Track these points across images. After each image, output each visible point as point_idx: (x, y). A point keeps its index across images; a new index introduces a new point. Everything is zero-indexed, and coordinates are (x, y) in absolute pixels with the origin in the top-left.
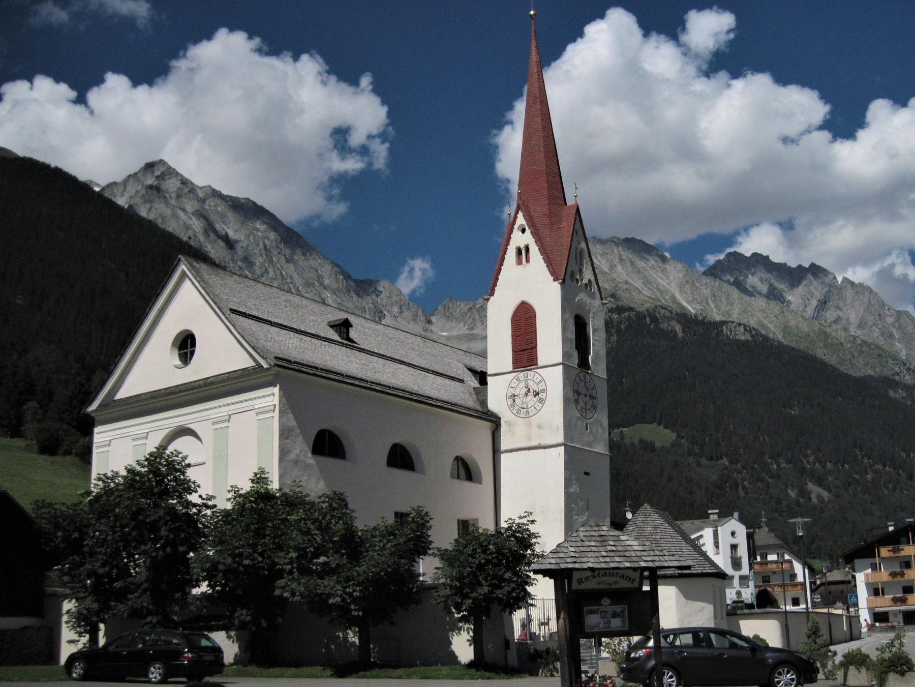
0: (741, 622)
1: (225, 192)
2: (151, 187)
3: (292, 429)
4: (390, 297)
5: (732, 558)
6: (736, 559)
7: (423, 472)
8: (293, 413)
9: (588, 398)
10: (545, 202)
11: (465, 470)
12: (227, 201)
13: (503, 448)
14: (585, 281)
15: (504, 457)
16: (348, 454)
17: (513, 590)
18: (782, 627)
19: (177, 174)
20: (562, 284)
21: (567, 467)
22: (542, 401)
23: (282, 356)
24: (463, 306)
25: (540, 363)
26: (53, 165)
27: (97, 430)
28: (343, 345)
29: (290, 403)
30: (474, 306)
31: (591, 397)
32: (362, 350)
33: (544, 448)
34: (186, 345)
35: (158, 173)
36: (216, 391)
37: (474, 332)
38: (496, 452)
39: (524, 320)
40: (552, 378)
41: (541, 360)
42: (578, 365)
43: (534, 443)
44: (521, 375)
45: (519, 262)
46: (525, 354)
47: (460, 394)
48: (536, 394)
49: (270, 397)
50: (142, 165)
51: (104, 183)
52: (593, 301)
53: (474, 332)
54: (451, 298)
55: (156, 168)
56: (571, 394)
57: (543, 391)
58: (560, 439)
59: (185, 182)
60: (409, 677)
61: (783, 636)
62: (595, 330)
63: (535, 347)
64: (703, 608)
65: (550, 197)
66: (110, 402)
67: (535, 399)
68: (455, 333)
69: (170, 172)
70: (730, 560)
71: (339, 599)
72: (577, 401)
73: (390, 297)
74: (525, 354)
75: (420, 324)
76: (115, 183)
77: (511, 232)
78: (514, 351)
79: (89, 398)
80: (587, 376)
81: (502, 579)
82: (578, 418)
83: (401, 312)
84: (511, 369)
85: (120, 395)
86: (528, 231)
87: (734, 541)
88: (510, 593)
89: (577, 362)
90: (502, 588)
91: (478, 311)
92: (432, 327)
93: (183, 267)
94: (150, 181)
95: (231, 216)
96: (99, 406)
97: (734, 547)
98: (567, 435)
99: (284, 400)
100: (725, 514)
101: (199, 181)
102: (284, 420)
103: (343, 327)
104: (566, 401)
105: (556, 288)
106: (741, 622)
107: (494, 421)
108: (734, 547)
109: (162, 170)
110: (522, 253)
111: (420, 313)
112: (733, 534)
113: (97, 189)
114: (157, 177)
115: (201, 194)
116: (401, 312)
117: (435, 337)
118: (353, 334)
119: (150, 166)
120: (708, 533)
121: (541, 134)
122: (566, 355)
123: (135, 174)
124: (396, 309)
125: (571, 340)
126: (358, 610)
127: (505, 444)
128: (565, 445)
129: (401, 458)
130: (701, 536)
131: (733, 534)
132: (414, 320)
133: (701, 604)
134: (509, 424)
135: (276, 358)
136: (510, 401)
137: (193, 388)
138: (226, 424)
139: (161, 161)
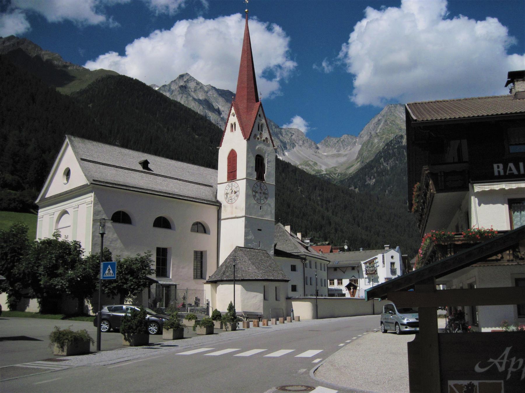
0: (293, 302)
1: (217, 88)
2: (182, 86)
3: (100, 212)
4: (298, 136)
5: (391, 269)
6: (394, 269)
7: (175, 230)
8: (101, 204)
9: (262, 194)
10: (245, 101)
11: (201, 228)
12: (218, 92)
13: (222, 218)
14: (264, 138)
15: (222, 222)
16: (133, 221)
17: (132, 285)
18: (313, 306)
19: (194, 80)
20: (247, 141)
21: (246, 227)
22: (237, 196)
23: (97, 179)
24: (334, 140)
25: (238, 178)
26: (134, 79)
27: (39, 211)
28: (144, 172)
29: (99, 200)
30: (340, 140)
31: (264, 193)
32: (156, 175)
33: (237, 218)
34: (68, 173)
35: (185, 80)
36: (74, 195)
37: (340, 152)
38: (219, 219)
39: (232, 157)
40: (241, 185)
41: (238, 177)
42: (256, 179)
43: (234, 216)
44: (230, 184)
45: (232, 131)
46: (232, 175)
47: (204, 193)
48: (235, 193)
49: (90, 197)
50: (178, 76)
51: (161, 85)
52: (268, 148)
53: (340, 152)
54: (328, 136)
55: (184, 77)
56: (250, 192)
57: (238, 191)
58: (243, 214)
59: (198, 83)
60: (76, 320)
61: (313, 310)
62: (268, 162)
63: (236, 171)
64: (257, 296)
65: (248, 99)
66: (43, 199)
67: (235, 195)
68: (330, 153)
69: (191, 79)
70: (390, 270)
71: (60, 287)
72: (254, 196)
73: (298, 136)
74: (232, 175)
75: (313, 149)
76: (165, 85)
77: (229, 116)
78: (228, 173)
79: (36, 198)
80: (262, 184)
81: (127, 280)
82: (255, 204)
83: (303, 144)
84: (226, 181)
85: (47, 196)
86: (235, 116)
87: (392, 261)
88: (130, 286)
89: (256, 177)
90: (127, 284)
91: (342, 142)
92: (319, 151)
93: (67, 140)
94: (182, 83)
95: (221, 100)
96: (40, 201)
97: (392, 264)
98: (246, 213)
99: (96, 199)
100: (392, 247)
101: (204, 82)
102: (96, 207)
103: (145, 164)
104: (247, 196)
105: (245, 142)
106: (293, 302)
107: (218, 205)
108: (392, 264)
109: (187, 78)
110: (233, 126)
111: (313, 143)
112: (392, 257)
113: (157, 89)
114: (185, 82)
115: (206, 89)
116: (303, 144)
117: (320, 155)
118: (150, 166)
119: (181, 76)
120: (380, 257)
121: (246, 69)
122: (248, 174)
123: (175, 80)
124: (301, 142)
125: (252, 167)
126: (69, 291)
127: (223, 216)
128: (245, 216)
129: (162, 223)
130: (376, 258)
131: (392, 257)
132: (310, 147)
133: (255, 293)
134: (225, 206)
135: (94, 180)
136: (225, 196)
137: (68, 193)
138: (77, 209)
139: (187, 74)
